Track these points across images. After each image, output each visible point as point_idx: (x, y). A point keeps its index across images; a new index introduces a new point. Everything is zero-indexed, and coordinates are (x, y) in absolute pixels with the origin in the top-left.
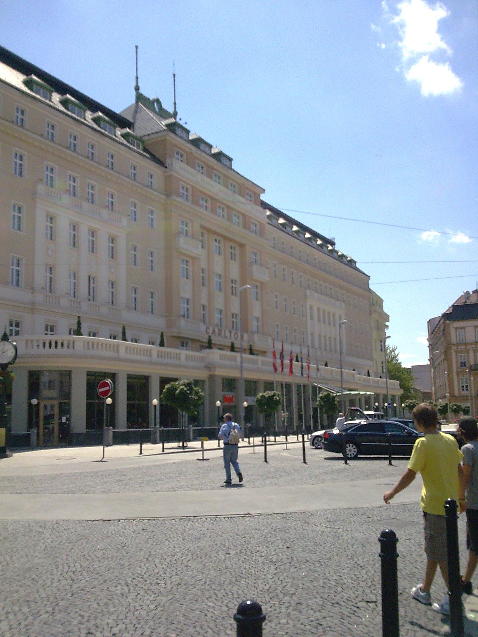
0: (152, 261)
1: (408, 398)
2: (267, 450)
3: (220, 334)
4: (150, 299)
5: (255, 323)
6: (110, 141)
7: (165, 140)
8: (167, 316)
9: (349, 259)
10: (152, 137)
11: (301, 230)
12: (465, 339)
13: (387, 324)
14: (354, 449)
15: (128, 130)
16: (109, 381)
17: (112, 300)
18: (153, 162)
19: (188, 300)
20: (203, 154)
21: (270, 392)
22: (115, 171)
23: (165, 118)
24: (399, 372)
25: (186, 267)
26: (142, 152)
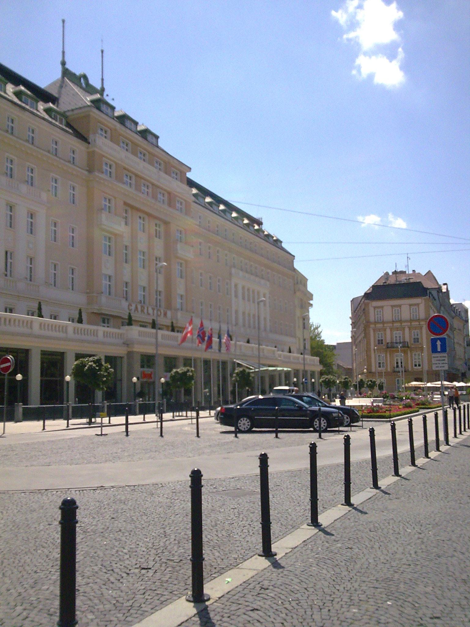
0: (73, 237)
1: (329, 373)
2: (163, 426)
3: (142, 311)
4: (71, 276)
5: (179, 301)
6: (31, 115)
7: (88, 117)
8: (87, 293)
9: (275, 238)
10: (76, 112)
11: (227, 210)
13: (311, 302)
14: (325, 423)
15: (51, 105)
16: (10, 357)
17: (55, 282)
18: (75, 138)
19: (110, 277)
20: (128, 131)
21: (184, 368)
22: (76, 166)
23: (91, 94)
24: (322, 349)
25: (108, 244)
26: (64, 127)
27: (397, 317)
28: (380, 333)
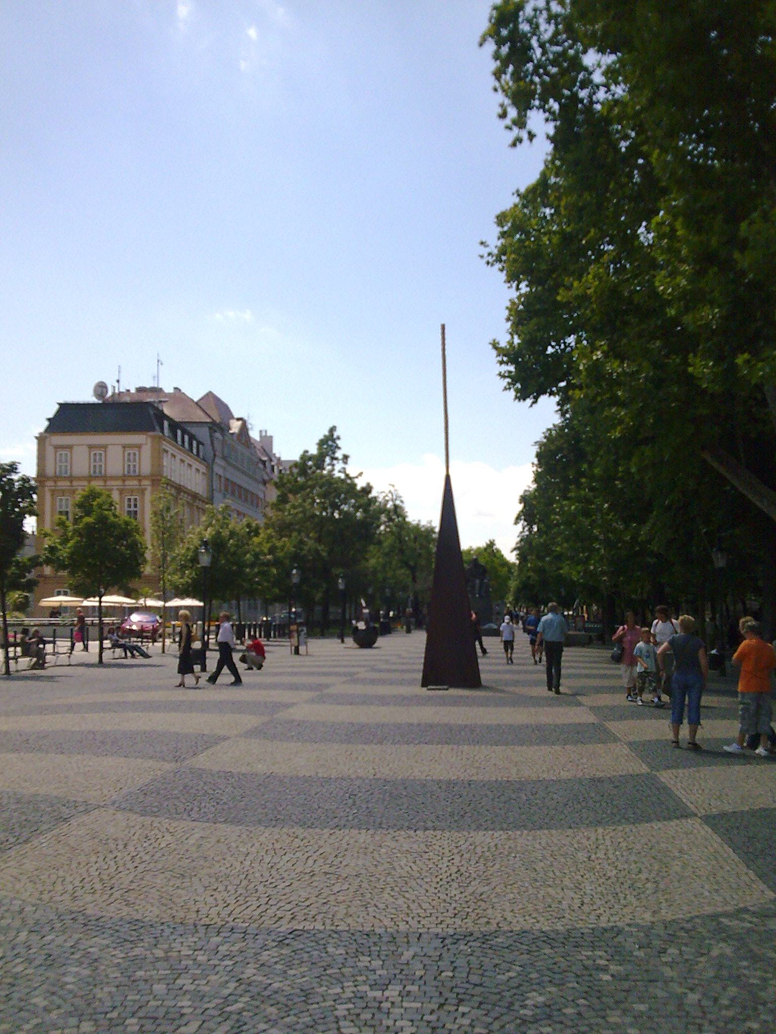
12: (105, 471)
13: (545, 440)
27: (63, 467)
28: (132, 498)
